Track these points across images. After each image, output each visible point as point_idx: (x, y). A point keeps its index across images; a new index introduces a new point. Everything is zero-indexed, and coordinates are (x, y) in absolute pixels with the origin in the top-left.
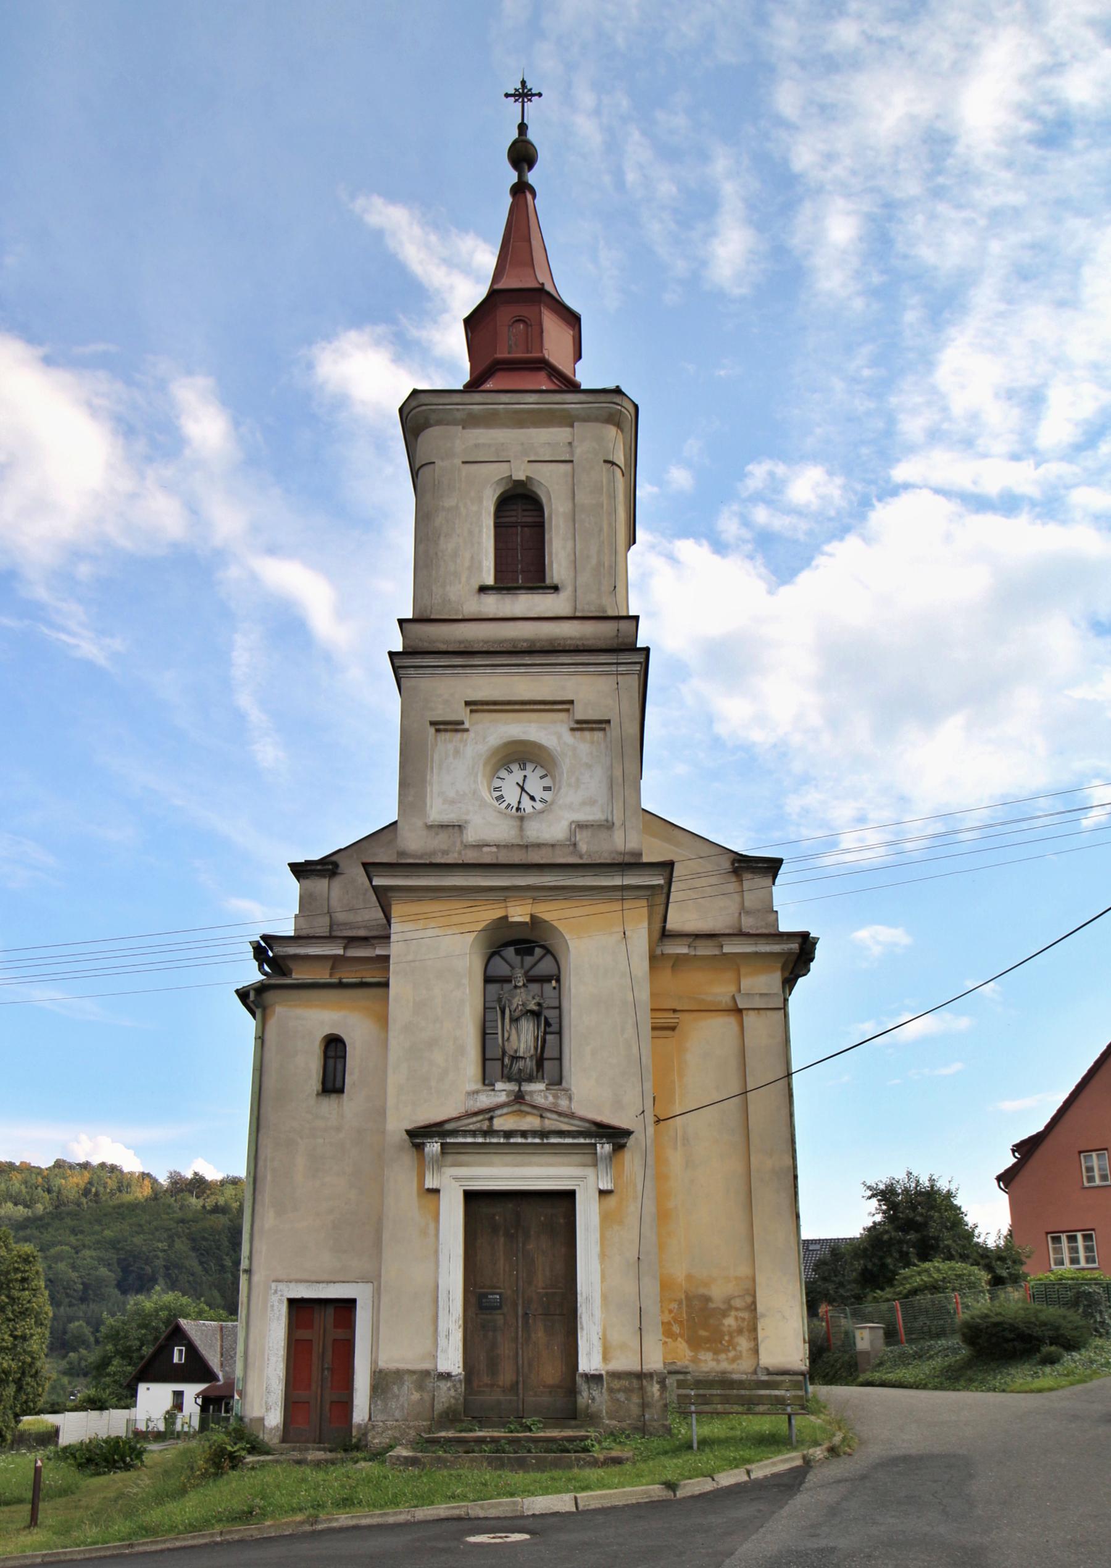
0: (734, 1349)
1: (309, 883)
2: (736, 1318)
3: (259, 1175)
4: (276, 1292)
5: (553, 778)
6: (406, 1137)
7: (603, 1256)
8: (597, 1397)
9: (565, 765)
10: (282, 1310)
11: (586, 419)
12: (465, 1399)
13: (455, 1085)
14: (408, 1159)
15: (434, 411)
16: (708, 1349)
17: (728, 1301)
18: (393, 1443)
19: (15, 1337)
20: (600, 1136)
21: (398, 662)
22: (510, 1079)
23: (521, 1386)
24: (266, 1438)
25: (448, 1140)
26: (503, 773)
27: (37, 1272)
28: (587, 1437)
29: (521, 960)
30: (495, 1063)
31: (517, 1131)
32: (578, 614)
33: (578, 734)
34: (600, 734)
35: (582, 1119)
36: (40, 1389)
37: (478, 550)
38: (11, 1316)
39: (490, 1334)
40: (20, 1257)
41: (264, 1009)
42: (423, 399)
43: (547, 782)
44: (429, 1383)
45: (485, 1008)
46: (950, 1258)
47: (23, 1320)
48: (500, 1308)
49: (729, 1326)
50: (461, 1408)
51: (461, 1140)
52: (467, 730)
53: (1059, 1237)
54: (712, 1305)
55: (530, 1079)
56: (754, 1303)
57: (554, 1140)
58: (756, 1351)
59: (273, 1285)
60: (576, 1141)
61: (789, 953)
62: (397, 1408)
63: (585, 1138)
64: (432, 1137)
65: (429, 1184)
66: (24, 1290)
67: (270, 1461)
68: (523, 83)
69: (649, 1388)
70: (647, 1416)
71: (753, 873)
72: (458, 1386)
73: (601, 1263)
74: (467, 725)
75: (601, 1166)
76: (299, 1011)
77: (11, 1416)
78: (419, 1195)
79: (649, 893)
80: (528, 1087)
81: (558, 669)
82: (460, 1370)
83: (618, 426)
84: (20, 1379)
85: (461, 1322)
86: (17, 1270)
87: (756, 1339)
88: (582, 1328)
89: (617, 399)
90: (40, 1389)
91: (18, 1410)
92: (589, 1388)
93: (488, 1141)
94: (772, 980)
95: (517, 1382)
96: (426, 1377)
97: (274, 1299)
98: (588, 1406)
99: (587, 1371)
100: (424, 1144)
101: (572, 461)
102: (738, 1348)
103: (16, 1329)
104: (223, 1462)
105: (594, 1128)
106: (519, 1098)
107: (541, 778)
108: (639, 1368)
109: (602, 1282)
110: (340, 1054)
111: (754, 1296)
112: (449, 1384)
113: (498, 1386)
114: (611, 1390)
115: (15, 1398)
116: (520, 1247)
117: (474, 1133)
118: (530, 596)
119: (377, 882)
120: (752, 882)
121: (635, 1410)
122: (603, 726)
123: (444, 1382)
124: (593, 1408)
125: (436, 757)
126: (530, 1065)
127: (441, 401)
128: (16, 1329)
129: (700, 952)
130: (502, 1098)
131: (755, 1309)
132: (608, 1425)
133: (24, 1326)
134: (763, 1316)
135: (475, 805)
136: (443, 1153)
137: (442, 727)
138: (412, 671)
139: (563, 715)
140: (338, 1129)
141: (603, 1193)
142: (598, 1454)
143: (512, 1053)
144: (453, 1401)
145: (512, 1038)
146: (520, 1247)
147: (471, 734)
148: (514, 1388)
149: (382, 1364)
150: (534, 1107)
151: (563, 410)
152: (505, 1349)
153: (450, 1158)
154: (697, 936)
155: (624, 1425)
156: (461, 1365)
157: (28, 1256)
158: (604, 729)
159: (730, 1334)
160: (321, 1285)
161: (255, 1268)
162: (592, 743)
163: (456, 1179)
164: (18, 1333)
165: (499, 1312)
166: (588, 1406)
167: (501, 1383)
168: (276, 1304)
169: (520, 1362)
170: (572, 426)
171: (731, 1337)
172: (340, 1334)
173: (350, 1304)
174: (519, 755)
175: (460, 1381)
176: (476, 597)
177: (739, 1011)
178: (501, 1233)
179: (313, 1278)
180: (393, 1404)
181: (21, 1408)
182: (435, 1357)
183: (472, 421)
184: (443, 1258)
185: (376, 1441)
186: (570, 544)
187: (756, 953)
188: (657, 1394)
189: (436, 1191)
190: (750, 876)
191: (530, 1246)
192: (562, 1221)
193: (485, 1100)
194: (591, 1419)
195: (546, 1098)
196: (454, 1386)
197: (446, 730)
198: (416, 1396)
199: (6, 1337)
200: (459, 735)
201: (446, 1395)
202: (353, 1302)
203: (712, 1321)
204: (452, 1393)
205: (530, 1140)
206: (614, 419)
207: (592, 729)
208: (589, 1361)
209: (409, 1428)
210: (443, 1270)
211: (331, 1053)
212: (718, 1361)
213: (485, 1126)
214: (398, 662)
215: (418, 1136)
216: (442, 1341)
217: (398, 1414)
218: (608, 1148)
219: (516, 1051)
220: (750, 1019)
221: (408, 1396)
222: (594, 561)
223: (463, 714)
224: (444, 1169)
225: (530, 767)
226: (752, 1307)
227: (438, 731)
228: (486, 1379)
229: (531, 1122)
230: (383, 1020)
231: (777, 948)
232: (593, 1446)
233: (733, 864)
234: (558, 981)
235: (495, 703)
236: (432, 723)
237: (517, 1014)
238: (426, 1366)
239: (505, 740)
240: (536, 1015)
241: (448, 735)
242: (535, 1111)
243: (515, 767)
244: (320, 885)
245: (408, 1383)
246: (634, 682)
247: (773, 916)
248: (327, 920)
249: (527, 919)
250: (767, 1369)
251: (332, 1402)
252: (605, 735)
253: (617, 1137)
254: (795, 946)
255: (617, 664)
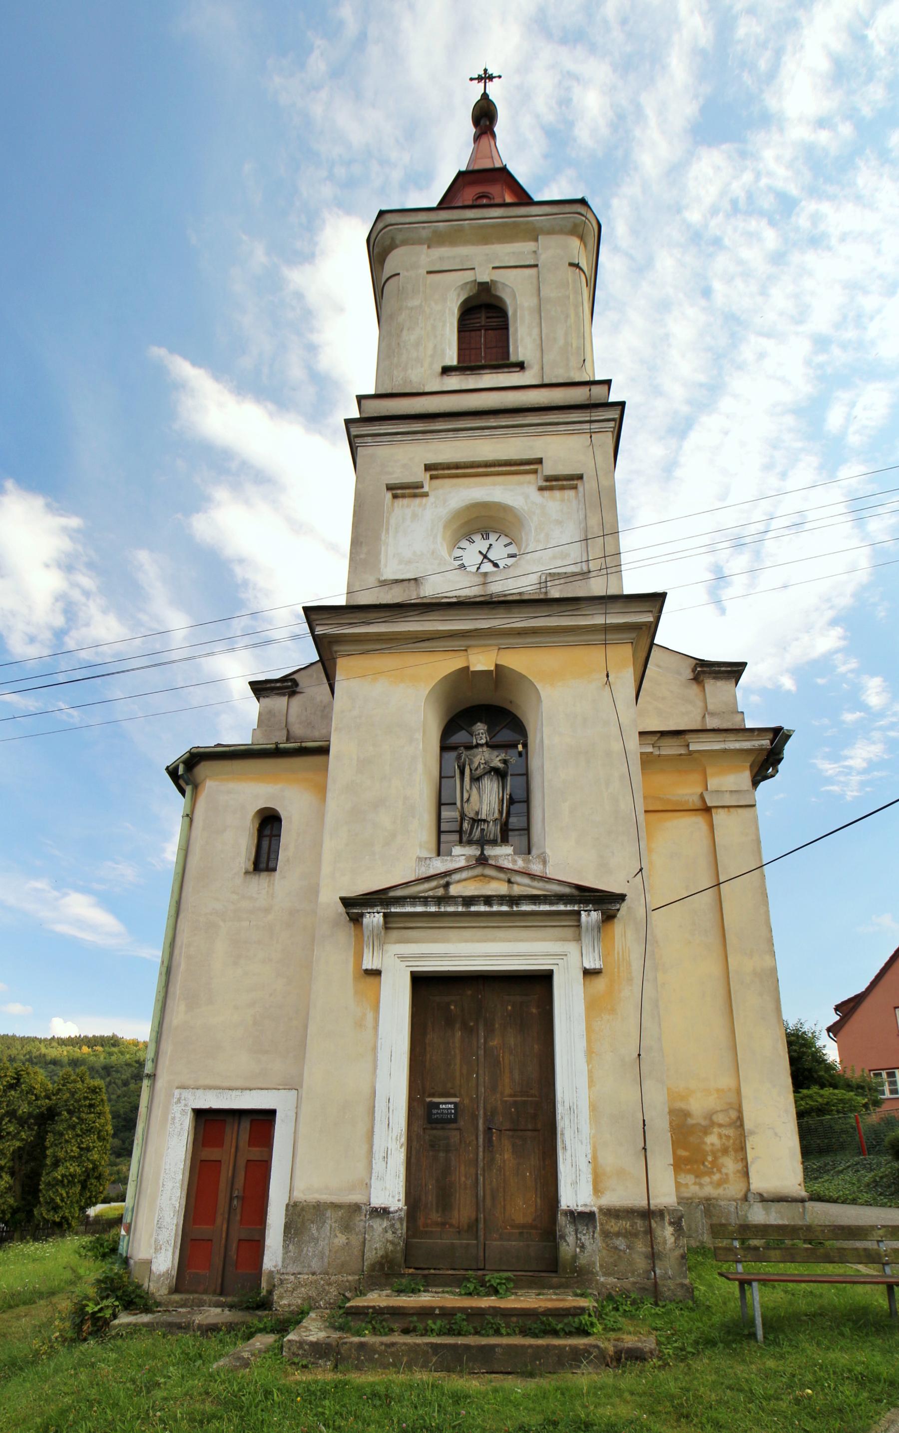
0: (720, 1171)
1: (266, 701)
2: (720, 1136)
3: (174, 963)
4: (179, 1100)
5: (519, 546)
6: (341, 908)
7: (590, 1053)
8: (587, 1243)
9: (533, 523)
10: (186, 1122)
11: (551, 232)
12: (407, 1244)
13: (405, 854)
14: (345, 934)
15: (400, 230)
16: (689, 1172)
17: (709, 1116)
18: (306, 1308)
19: (81, 1149)
20: (586, 902)
21: (354, 431)
22: (470, 842)
23: (481, 1226)
24: (153, 1288)
25: (393, 910)
26: (464, 544)
27: (102, 1100)
28: (582, 1310)
29: (484, 722)
30: (455, 827)
31: (479, 897)
32: (546, 381)
33: (547, 493)
34: (571, 493)
35: (560, 882)
36: (101, 1188)
37: (439, 337)
38: (79, 1132)
39: (442, 1155)
40: (89, 1088)
41: (196, 787)
42: (389, 219)
43: (512, 549)
44: (360, 1222)
45: (441, 777)
46: (822, 1086)
47: (89, 1136)
48: (455, 1121)
49: (712, 1144)
50: (400, 1257)
51: (409, 909)
52: (426, 495)
53: (880, 1074)
54: (690, 1121)
55: (494, 843)
56: (740, 1118)
57: (525, 908)
58: (746, 1174)
59: (177, 1092)
60: (554, 908)
61: (760, 750)
62: (314, 1255)
63: (565, 904)
64: (373, 906)
65: (367, 964)
66: (90, 1113)
67: (146, 1325)
68: (486, 70)
69: (658, 1232)
70: (658, 1271)
71: (714, 678)
72: (398, 1225)
73: (589, 1062)
74: (426, 489)
75: (586, 940)
76: (231, 785)
77: (77, 1209)
78: (356, 979)
79: (633, 635)
80: (490, 851)
81: (526, 430)
82: (401, 1204)
83: (582, 238)
84: (85, 1181)
85: (404, 1139)
86: (86, 1098)
87: (744, 1159)
88: (565, 1148)
89: (581, 209)
90: (101, 1188)
91: (82, 1204)
92: (576, 1231)
93: (442, 909)
94: (745, 777)
95: (477, 1220)
96: (352, 1212)
97: (176, 1109)
98: (575, 1257)
99: (573, 1207)
100: (362, 915)
101: (536, 266)
102: (724, 1170)
103: (82, 1143)
104: (89, 1325)
105: (575, 892)
106: (482, 861)
107: (505, 546)
108: (644, 1203)
109: (590, 1087)
110: (274, 832)
111: (740, 1111)
112: (385, 1224)
113: (451, 1225)
114: (606, 1235)
115: (81, 1195)
116: (482, 1042)
117: (425, 901)
118: (494, 375)
119: (319, 630)
120: (716, 689)
121: (641, 1264)
122: (575, 482)
123: (378, 1221)
124: (583, 1260)
125: (393, 521)
126: (493, 830)
127: (408, 220)
128: (82, 1143)
129: (664, 752)
130: (462, 863)
131: (742, 1125)
132: (603, 1284)
133: (90, 1140)
134: (752, 1133)
135: (426, 554)
136: (387, 927)
137: (399, 492)
138: (369, 439)
139: (531, 477)
140: (267, 910)
141: (588, 973)
142: (600, 1340)
143: (472, 815)
144: (390, 1247)
145: (472, 799)
146: (482, 1042)
147: (431, 499)
148: (472, 1228)
149: (298, 1196)
150: (500, 869)
151: (527, 223)
152: (461, 1175)
153: (394, 934)
154: (663, 734)
155: (627, 1284)
156: (402, 1196)
157: (96, 1088)
158: (575, 487)
159: (714, 1153)
160: (234, 1093)
161: (159, 1072)
162: (563, 500)
163: (402, 958)
164: (84, 1146)
165: (453, 1126)
166: (575, 1257)
167: (454, 1221)
168: (178, 1115)
169: (481, 1193)
170: (536, 240)
171: (716, 1158)
172: (255, 1153)
173: (267, 1117)
174: (483, 522)
175: (401, 1219)
176: (438, 379)
177: (707, 810)
178: (457, 1026)
179: (226, 1084)
180: (309, 1250)
181: (86, 1202)
182: (368, 1186)
183: (437, 240)
184: (383, 1056)
185: (284, 1302)
186: (536, 331)
187: (725, 751)
188: (671, 1240)
189: (377, 973)
190: (712, 681)
191: (495, 1043)
192: (534, 1011)
193: (439, 865)
194: (578, 1277)
195: (514, 862)
196: (393, 1226)
197: (403, 496)
198: (341, 1239)
199: (74, 1148)
200: (417, 501)
201: (380, 1239)
202: (272, 1113)
203: (692, 1139)
204: (390, 1236)
205: (495, 908)
206: (577, 231)
207: (562, 488)
208: (575, 1192)
209: (330, 1284)
210: (382, 1072)
211: (267, 832)
212: (701, 1185)
213: (440, 892)
214: (354, 431)
215: (355, 906)
216: (378, 1165)
217: (315, 1265)
218: (595, 916)
219: (477, 813)
220: (719, 817)
221: (330, 1239)
222: (561, 342)
223: (422, 476)
224: (388, 947)
225: (493, 537)
226: (739, 1123)
227: (395, 497)
228: (435, 1216)
229: (498, 888)
230: (322, 790)
231: (747, 745)
232: (592, 1325)
233: (694, 670)
234: (525, 746)
235: (457, 466)
236: (390, 488)
237: (479, 772)
238: (356, 1198)
239: (467, 503)
240: (500, 774)
241: (406, 501)
242: (502, 876)
243: (477, 538)
244: (279, 703)
245: (332, 1219)
246: (609, 439)
247: (739, 717)
248: (285, 732)
249: (492, 668)
250: (761, 1195)
251: (240, 1240)
252: (577, 493)
253: (607, 903)
254: (766, 743)
255: (591, 422)
